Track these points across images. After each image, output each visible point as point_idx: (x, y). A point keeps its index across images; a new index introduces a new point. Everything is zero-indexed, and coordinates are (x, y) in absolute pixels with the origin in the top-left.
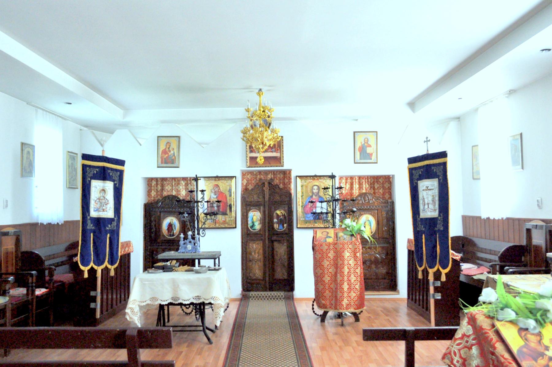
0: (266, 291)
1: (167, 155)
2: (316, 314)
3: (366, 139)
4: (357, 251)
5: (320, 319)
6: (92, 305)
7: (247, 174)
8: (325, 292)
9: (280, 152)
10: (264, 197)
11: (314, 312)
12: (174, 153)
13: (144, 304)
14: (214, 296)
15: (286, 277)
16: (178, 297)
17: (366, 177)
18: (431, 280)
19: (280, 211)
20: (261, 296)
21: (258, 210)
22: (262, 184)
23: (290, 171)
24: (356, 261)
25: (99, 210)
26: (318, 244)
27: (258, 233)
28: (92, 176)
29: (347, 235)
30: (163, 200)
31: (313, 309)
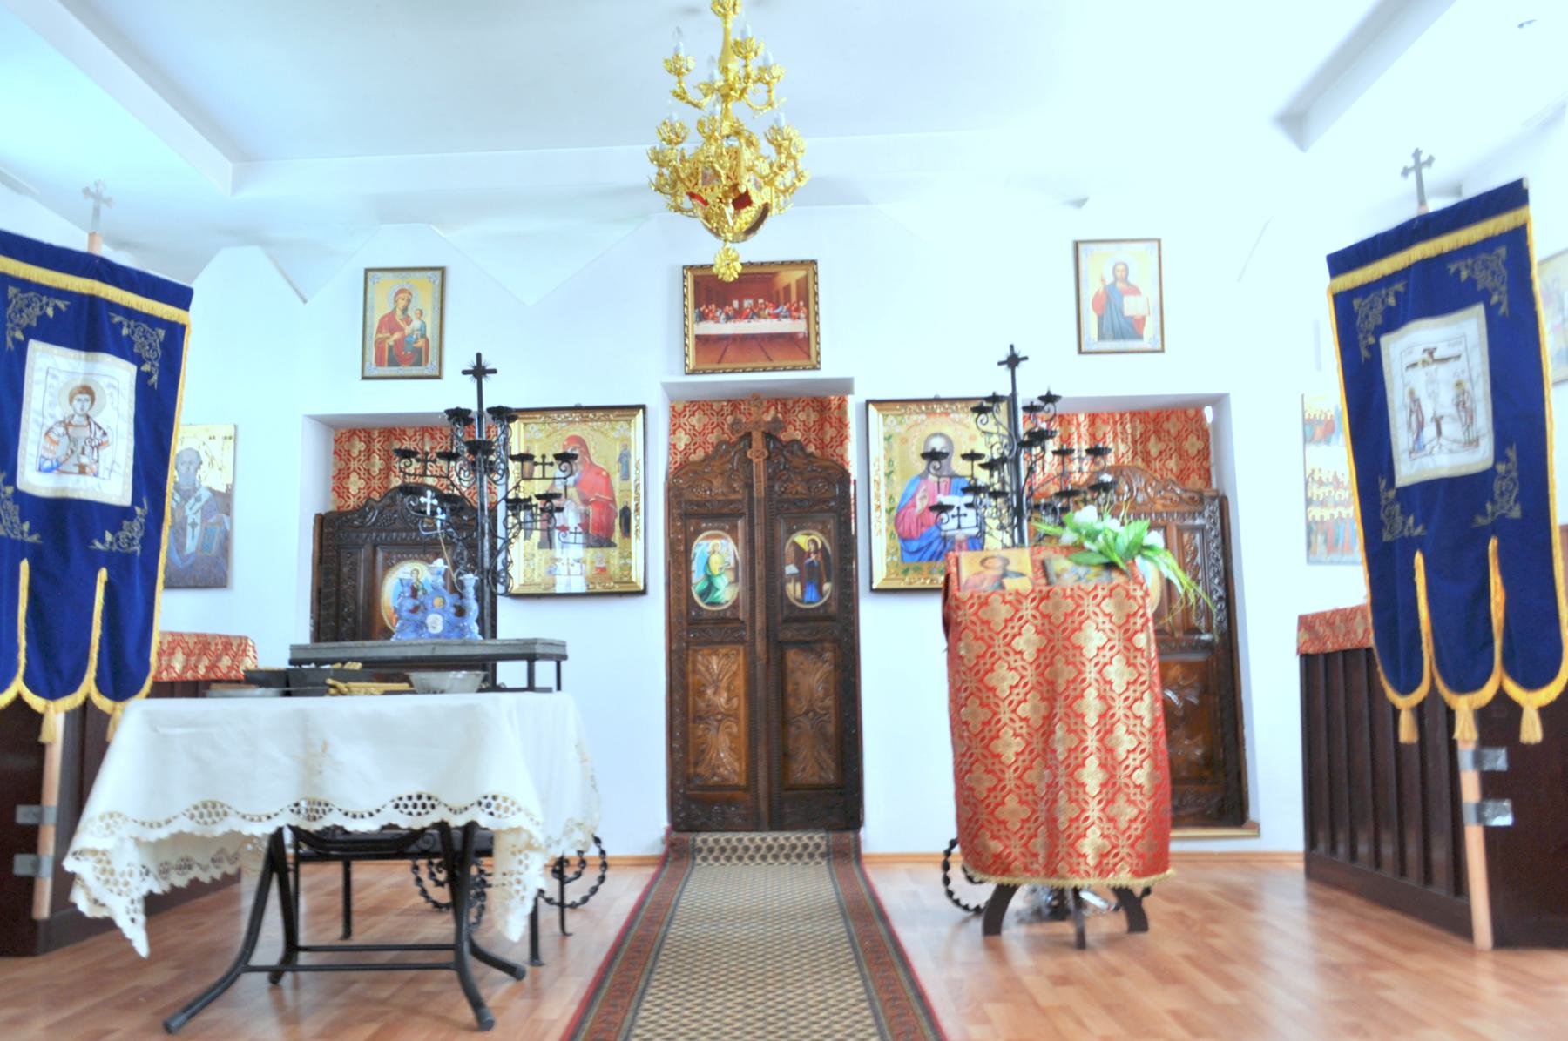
0: (756, 829)
1: (397, 336)
2: (957, 902)
3: (1121, 267)
4: (1138, 626)
5: (977, 925)
6: (22, 864)
7: (688, 413)
8: (1003, 803)
9: (808, 318)
10: (749, 486)
11: (950, 894)
12: (423, 328)
13: (163, 833)
14: (490, 791)
15: (831, 777)
16: (322, 798)
17: (1117, 417)
18: (1466, 741)
19: (809, 535)
20: (740, 847)
21: (729, 532)
22: (742, 438)
23: (844, 387)
24: (1134, 665)
25: (61, 468)
26: (971, 597)
27: (728, 614)
28: (34, 323)
29: (1089, 565)
30: (388, 501)
31: (947, 881)
